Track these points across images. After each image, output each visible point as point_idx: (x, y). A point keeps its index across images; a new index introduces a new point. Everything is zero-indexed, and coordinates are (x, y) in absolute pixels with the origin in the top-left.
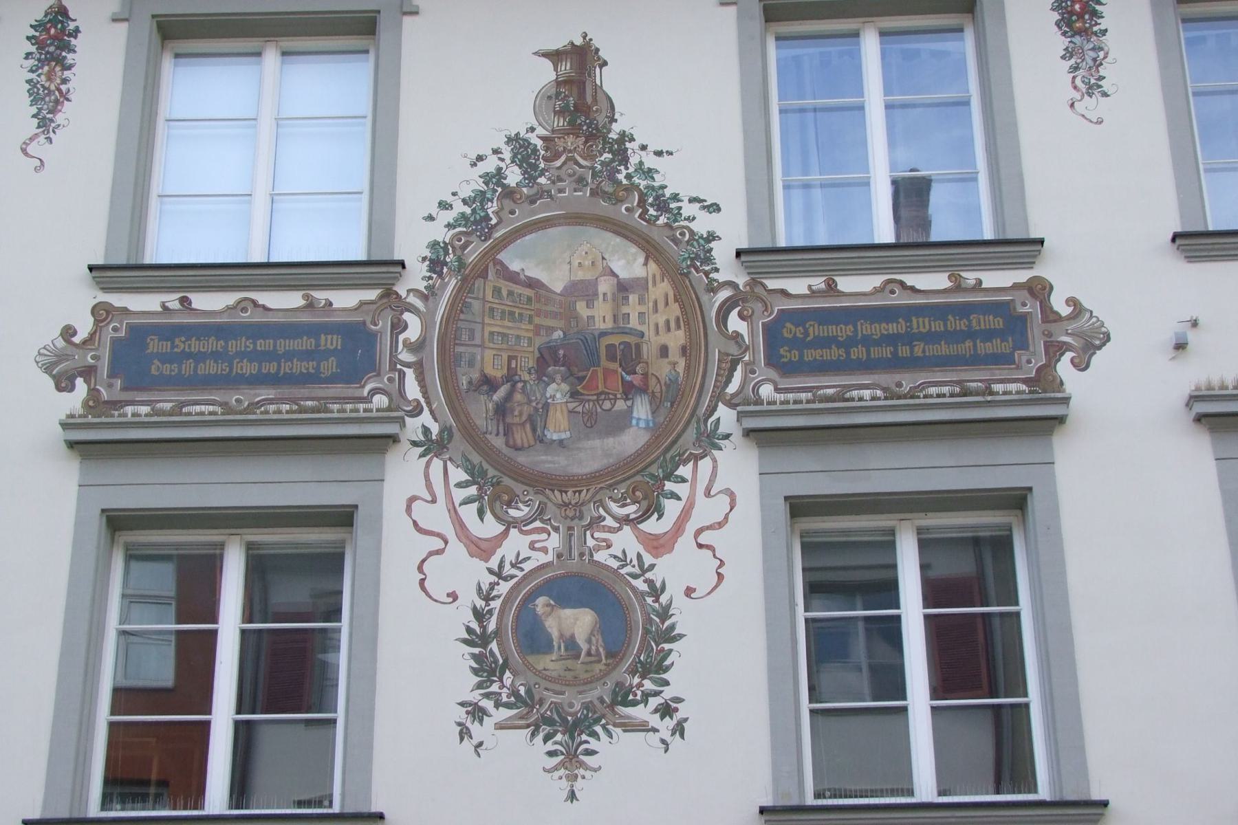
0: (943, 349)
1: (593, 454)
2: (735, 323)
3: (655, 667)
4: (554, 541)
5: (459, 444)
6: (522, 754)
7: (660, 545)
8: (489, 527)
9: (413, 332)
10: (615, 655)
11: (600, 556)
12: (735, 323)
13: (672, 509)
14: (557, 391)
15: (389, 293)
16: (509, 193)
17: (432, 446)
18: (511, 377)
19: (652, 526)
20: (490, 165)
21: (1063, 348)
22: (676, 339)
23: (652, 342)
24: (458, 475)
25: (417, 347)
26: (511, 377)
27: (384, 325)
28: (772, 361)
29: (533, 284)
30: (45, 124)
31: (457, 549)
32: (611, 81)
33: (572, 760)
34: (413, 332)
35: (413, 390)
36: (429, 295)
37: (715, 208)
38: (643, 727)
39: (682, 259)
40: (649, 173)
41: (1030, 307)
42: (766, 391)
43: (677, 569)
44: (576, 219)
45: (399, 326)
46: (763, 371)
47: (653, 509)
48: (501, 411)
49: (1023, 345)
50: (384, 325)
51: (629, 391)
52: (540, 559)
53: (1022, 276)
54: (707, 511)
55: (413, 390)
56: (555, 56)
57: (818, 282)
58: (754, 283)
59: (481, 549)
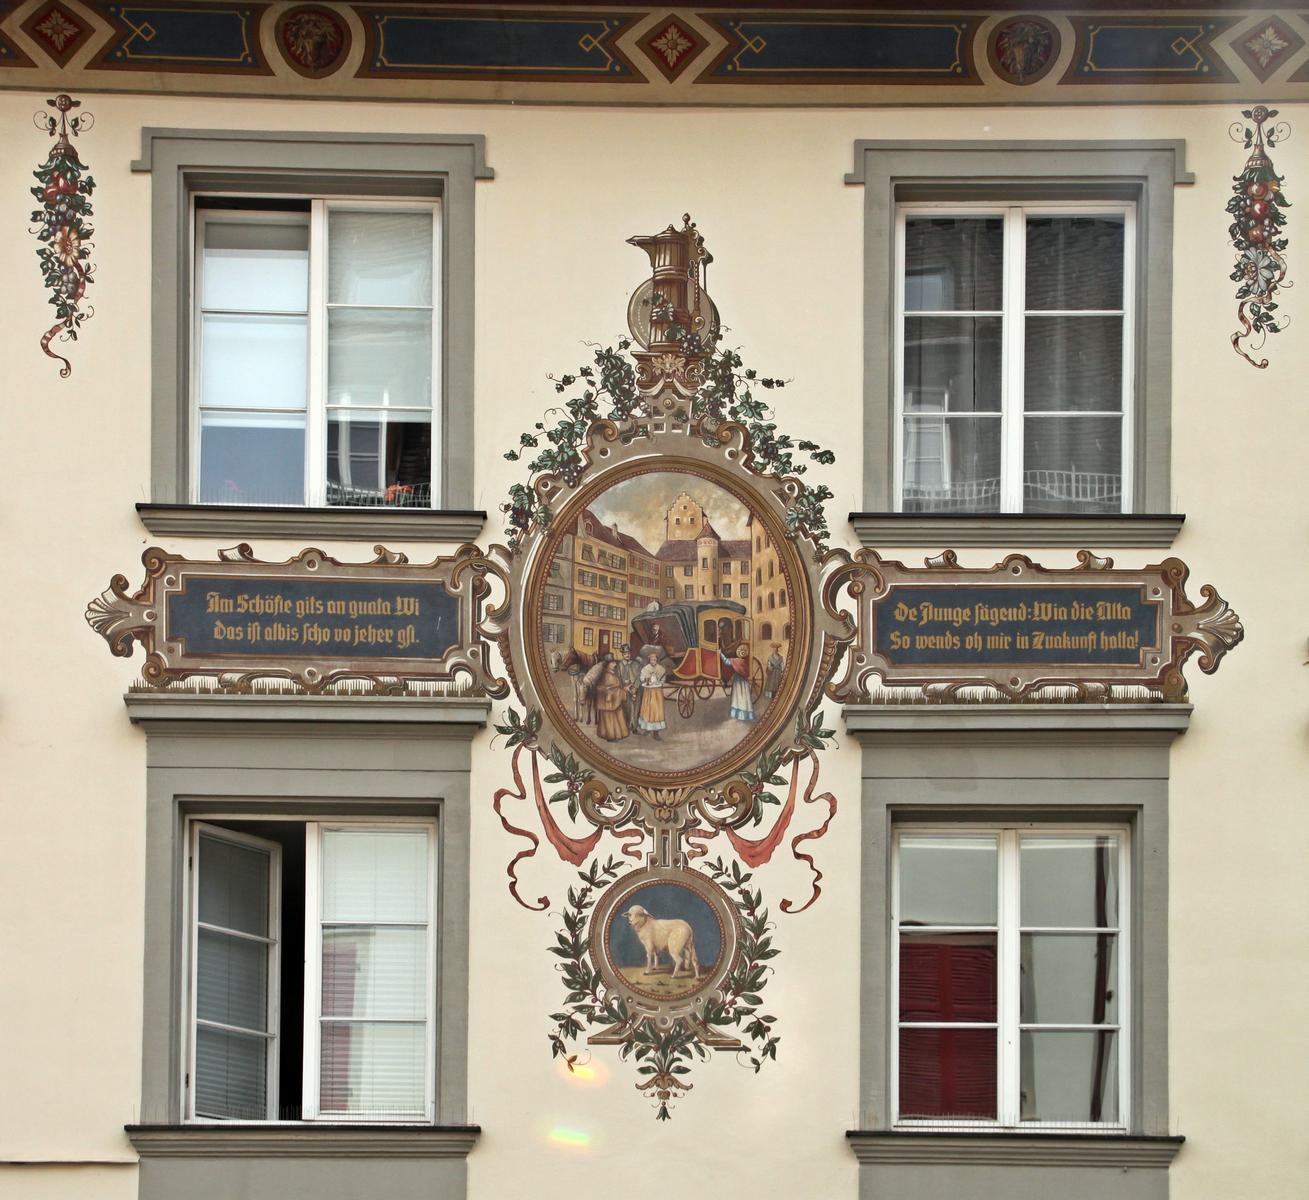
0: (1064, 642)
1: (692, 748)
2: (845, 601)
3: (749, 984)
4: (648, 845)
5: (548, 732)
6: (605, 1069)
7: (757, 853)
8: (579, 828)
9: (497, 598)
10: (708, 970)
11: (696, 864)
12: (845, 601)
13: (770, 813)
14: (652, 674)
15: (469, 550)
16: (600, 427)
17: (521, 734)
18: (603, 654)
19: (749, 832)
20: (578, 390)
21: (1194, 645)
22: (780, 617)
23: (755, 618)
24: (548, 768)
25: (501, 616)
26: (603, 654)
27: (464, 588)
28: (882, 647)
29: (627, 543)
30: (66, 312)
31: (547, 850)
32: (716, 282)
33: (664, 1079)
34: (497, 598)
35: (498, 668)
36: (513, 553)
37: (827, 457)
38: (735, 1046)
39: (792, 517)
40: (757, 408)
41: (1162, 596)
42: (874, 684)
43: (775, 879)
44: (674, 464)
45: (481, 591)
46: (871, 660)
47: (751, 813)
48: (593, 695)
49: (1149, 640)
50: (464, 588)
51: (729, 677)
52: (633, 864)
53: (1157, 557)
54: (807, 817)
55: (498, 668)
56: (651, 245)
57: (936, 555)
58: (866, 553)
59: (573, 851)
